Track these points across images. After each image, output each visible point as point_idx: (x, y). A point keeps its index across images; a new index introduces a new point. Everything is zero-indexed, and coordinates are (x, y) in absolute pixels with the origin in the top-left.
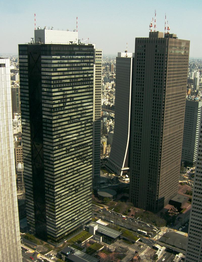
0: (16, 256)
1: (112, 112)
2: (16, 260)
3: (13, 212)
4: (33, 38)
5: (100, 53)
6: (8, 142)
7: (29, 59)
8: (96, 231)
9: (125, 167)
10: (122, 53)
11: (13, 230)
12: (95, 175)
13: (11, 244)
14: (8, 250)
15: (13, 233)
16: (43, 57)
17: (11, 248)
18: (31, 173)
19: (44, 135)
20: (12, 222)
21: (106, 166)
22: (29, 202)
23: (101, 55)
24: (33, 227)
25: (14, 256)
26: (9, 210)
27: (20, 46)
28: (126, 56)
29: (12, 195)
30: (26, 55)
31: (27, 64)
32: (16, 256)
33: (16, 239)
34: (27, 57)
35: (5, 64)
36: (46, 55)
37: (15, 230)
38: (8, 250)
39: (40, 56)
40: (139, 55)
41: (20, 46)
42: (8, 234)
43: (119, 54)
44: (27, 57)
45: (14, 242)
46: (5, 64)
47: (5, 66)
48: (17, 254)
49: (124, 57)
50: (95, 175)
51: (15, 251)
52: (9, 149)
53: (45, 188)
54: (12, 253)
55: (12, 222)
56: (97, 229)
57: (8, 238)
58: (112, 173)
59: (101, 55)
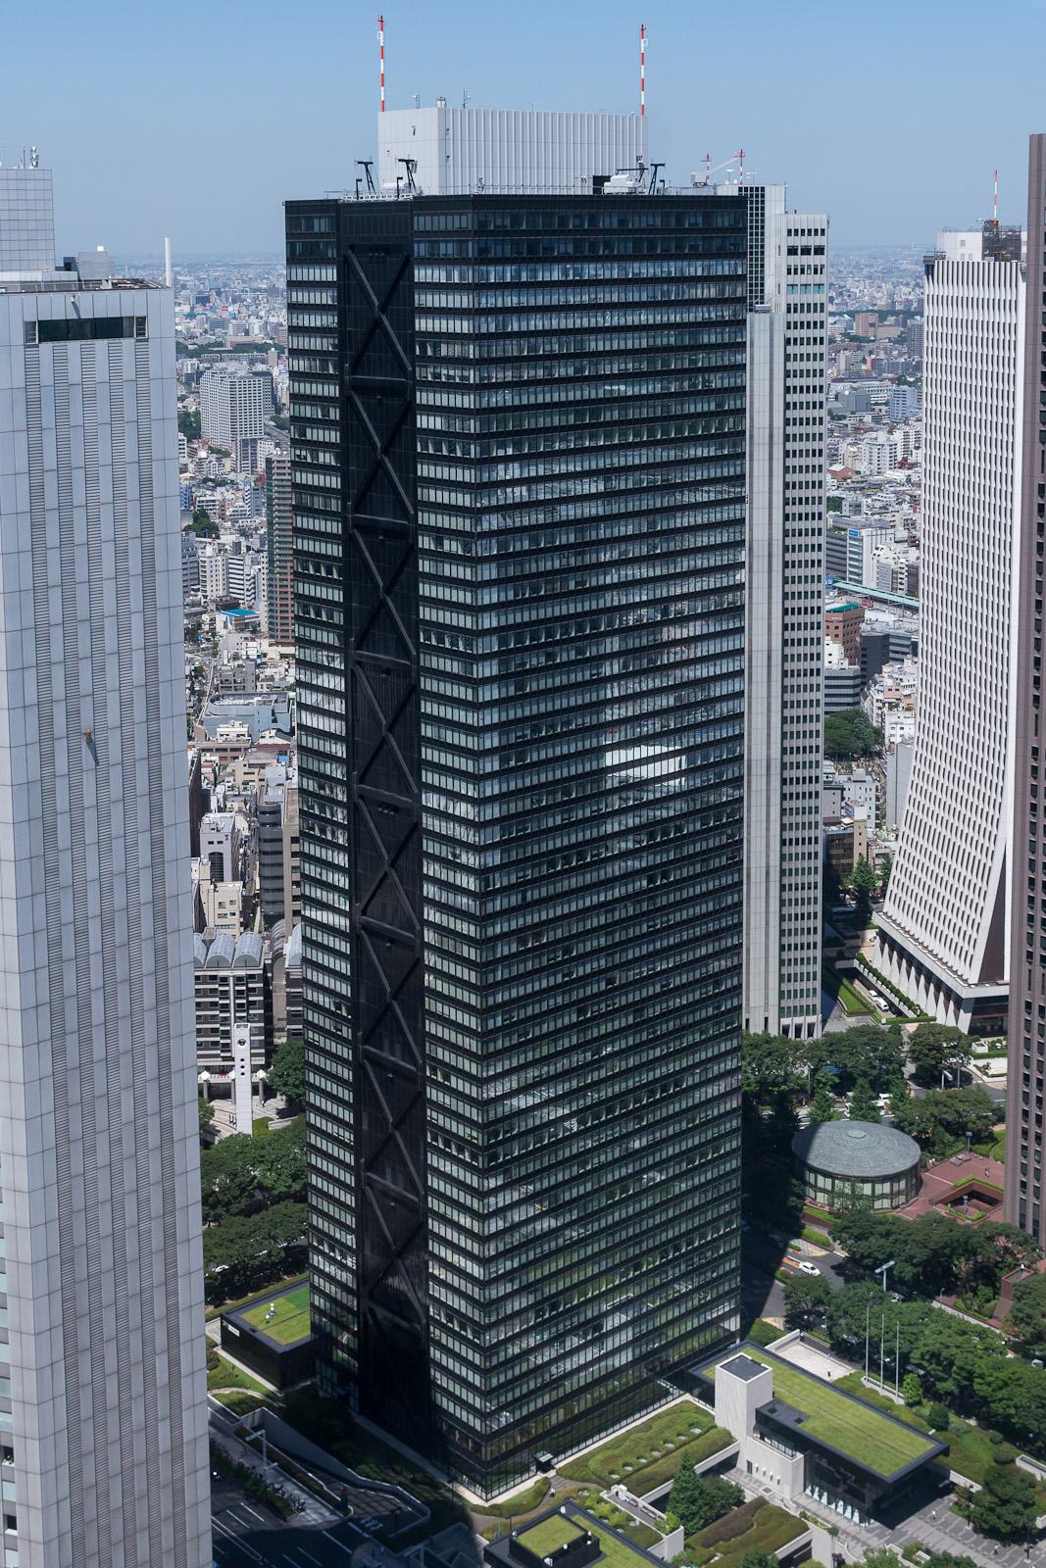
3: (170, 1236)
4: (366, 164)
5: (813, 241)
6: (155, 787)
12: (786, 1021)
15: (162, 1377)
19: (428, 731)
20: (159, 1309)
22: (620, 608)
23: (820, 251)
24: (343, 1347)
27: (294, 209)
29: (166, 1127)
30: (323, 261)
33: (176, 1426)
34: (330, 274)
35: (142, 321)
39: (407, 266)
40: (890, 330)
41: (294, 209)
44: (330, 274)
46: (142, 321)
47: (141, 332)
50: (786, 1021)
53: (356, 1160)
57: (124, 1413)
59: (820, 251)
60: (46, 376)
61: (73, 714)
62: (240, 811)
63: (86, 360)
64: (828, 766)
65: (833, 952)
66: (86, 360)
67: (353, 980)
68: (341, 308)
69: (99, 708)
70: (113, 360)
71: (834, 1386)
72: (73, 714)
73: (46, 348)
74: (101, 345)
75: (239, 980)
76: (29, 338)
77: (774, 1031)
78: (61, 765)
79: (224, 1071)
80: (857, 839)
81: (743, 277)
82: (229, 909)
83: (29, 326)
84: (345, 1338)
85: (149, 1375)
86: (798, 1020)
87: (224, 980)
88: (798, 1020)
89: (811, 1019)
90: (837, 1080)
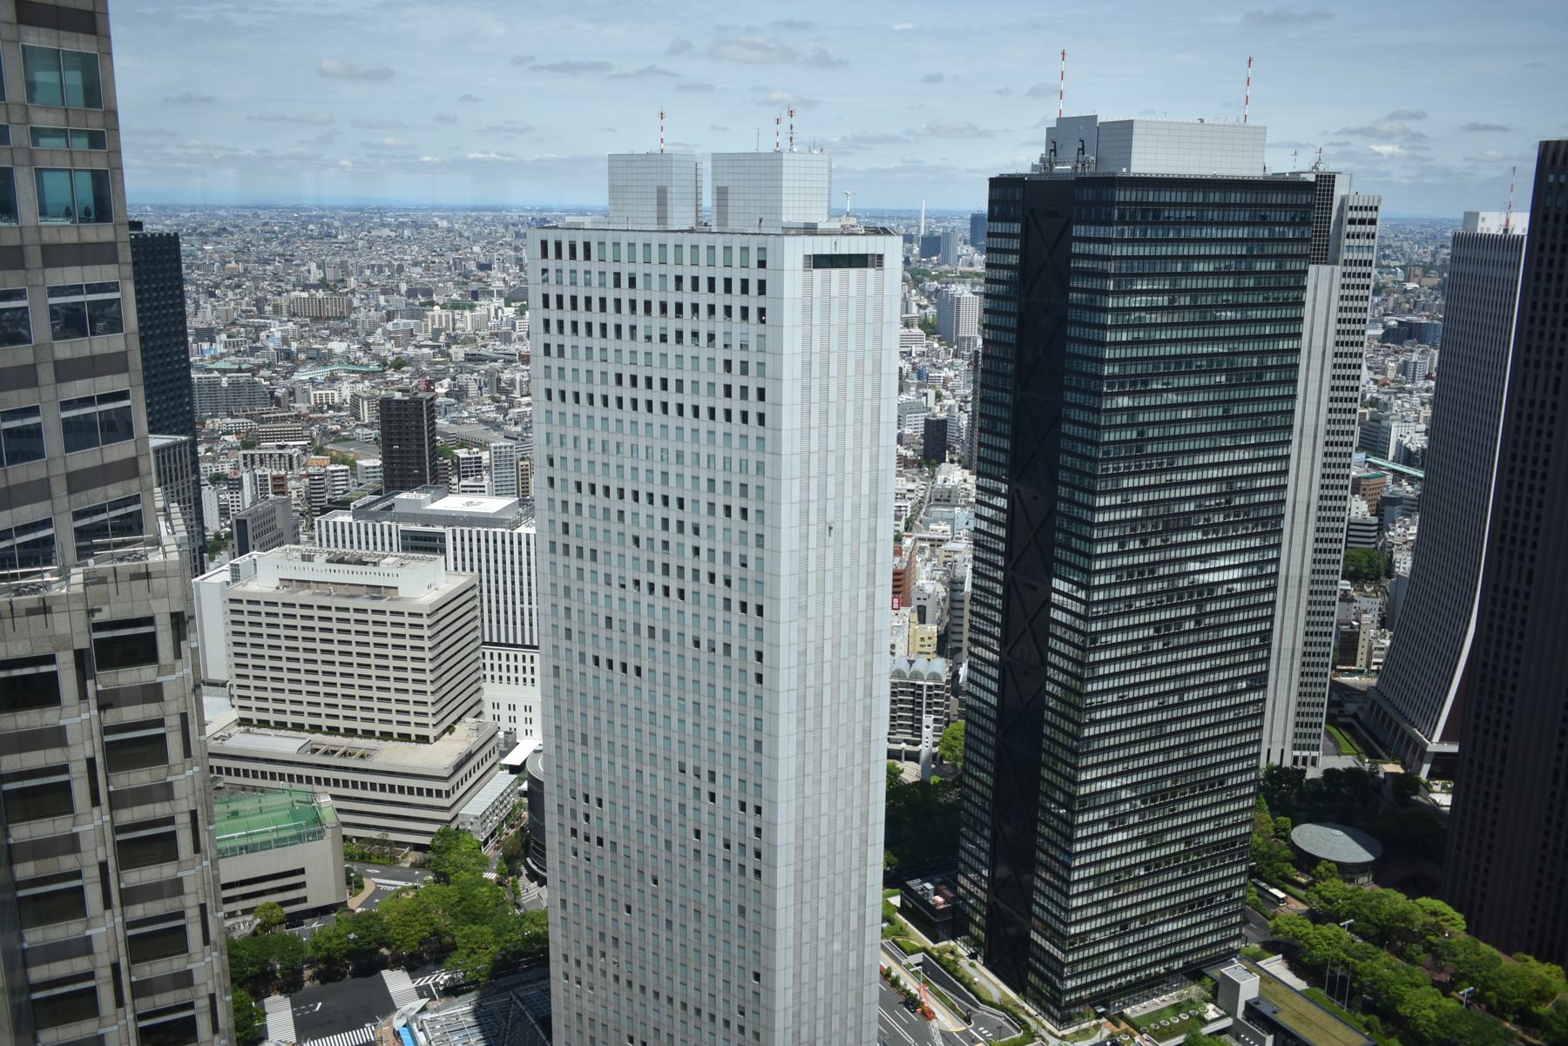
0: (851, 1022)
1: (433, 431)
2: (850, 1040)
3: (864, 841)
7: (1024, 237)
8: (1247, 1003)
9: (1443, 739)
10: (1482, 215)
11: (854, 917)
12: (1297, 753)
13: (837, 968)
14: (821, 993)
15: (854, 925)
16: (1079, 230)
17: (836, 987)
18: (993, 700)
20: (855, 884)
21: (1359, 721)
23: (1373, 222)
24: (978, 925)
25: (843, 1021)
26: (848, 833)
28: (1506, 231)
30: (1013, 220)
31: (1014, 259)
32: (851, 1022)
34: (1016, 228)
35: (880, 257)
36: (1098, 222)
37: (862, 918)
38: (821, 993)
42: (830, 926)
43: (1471, 217)
44: (1016, 228)
45: (853, 964)
46: (880, 257)
48: (859, 1017)
49: (1493, 231)
50: (1297, 753)
51: (852, 1002)
52: (871, 589)
54: (836, 1006)
55: (855, 884)
56: (1255, 995)
58: (1379, 757)
59: (1373, 222)
60: (835, 291)
61: (823, 511)
62: (940, 580)
63: (845, 282)
64: (1345, 585)
65: (1335, 711)
66: (845, 282)
67: (1000, 695)
68: (1023, 252)
69: (840, 509)
70: (863, 283)
71: (1300, 993)
72: (823, 511)
73: (818, 273)
74: (853, 272)
75: (929, 687)
76: (807, 267)
77: (1288, 763)
78: (813, 543)
79: (916, 744)
80: (1362, 636)
81: (1309, 240)
82: (927, 642)
83: (807, 257)
84: (978, 918)
85: (846, 923)
86: (1306, 753)
87: (920, 687)
88: (1306, 753)
89: (1315, 754)
90: (398, 982)
